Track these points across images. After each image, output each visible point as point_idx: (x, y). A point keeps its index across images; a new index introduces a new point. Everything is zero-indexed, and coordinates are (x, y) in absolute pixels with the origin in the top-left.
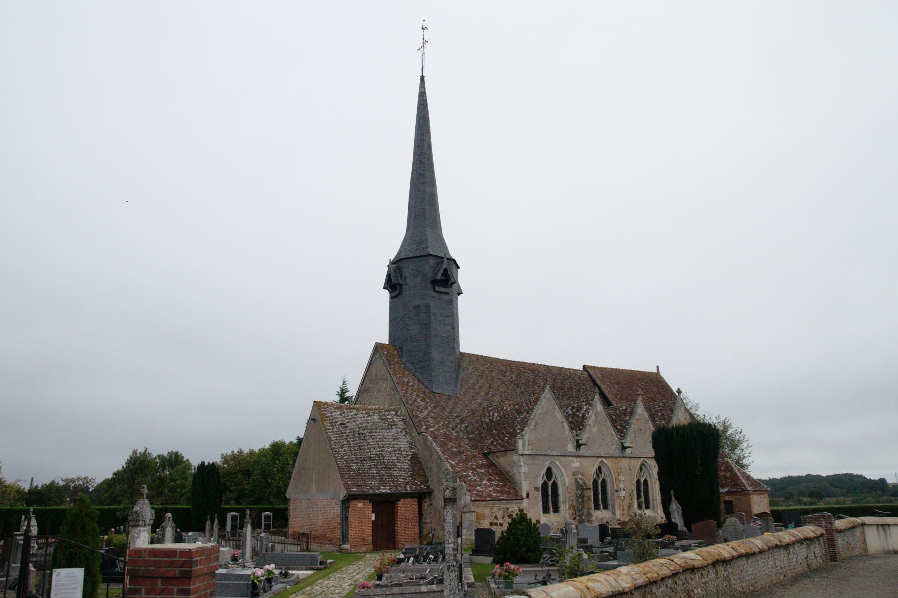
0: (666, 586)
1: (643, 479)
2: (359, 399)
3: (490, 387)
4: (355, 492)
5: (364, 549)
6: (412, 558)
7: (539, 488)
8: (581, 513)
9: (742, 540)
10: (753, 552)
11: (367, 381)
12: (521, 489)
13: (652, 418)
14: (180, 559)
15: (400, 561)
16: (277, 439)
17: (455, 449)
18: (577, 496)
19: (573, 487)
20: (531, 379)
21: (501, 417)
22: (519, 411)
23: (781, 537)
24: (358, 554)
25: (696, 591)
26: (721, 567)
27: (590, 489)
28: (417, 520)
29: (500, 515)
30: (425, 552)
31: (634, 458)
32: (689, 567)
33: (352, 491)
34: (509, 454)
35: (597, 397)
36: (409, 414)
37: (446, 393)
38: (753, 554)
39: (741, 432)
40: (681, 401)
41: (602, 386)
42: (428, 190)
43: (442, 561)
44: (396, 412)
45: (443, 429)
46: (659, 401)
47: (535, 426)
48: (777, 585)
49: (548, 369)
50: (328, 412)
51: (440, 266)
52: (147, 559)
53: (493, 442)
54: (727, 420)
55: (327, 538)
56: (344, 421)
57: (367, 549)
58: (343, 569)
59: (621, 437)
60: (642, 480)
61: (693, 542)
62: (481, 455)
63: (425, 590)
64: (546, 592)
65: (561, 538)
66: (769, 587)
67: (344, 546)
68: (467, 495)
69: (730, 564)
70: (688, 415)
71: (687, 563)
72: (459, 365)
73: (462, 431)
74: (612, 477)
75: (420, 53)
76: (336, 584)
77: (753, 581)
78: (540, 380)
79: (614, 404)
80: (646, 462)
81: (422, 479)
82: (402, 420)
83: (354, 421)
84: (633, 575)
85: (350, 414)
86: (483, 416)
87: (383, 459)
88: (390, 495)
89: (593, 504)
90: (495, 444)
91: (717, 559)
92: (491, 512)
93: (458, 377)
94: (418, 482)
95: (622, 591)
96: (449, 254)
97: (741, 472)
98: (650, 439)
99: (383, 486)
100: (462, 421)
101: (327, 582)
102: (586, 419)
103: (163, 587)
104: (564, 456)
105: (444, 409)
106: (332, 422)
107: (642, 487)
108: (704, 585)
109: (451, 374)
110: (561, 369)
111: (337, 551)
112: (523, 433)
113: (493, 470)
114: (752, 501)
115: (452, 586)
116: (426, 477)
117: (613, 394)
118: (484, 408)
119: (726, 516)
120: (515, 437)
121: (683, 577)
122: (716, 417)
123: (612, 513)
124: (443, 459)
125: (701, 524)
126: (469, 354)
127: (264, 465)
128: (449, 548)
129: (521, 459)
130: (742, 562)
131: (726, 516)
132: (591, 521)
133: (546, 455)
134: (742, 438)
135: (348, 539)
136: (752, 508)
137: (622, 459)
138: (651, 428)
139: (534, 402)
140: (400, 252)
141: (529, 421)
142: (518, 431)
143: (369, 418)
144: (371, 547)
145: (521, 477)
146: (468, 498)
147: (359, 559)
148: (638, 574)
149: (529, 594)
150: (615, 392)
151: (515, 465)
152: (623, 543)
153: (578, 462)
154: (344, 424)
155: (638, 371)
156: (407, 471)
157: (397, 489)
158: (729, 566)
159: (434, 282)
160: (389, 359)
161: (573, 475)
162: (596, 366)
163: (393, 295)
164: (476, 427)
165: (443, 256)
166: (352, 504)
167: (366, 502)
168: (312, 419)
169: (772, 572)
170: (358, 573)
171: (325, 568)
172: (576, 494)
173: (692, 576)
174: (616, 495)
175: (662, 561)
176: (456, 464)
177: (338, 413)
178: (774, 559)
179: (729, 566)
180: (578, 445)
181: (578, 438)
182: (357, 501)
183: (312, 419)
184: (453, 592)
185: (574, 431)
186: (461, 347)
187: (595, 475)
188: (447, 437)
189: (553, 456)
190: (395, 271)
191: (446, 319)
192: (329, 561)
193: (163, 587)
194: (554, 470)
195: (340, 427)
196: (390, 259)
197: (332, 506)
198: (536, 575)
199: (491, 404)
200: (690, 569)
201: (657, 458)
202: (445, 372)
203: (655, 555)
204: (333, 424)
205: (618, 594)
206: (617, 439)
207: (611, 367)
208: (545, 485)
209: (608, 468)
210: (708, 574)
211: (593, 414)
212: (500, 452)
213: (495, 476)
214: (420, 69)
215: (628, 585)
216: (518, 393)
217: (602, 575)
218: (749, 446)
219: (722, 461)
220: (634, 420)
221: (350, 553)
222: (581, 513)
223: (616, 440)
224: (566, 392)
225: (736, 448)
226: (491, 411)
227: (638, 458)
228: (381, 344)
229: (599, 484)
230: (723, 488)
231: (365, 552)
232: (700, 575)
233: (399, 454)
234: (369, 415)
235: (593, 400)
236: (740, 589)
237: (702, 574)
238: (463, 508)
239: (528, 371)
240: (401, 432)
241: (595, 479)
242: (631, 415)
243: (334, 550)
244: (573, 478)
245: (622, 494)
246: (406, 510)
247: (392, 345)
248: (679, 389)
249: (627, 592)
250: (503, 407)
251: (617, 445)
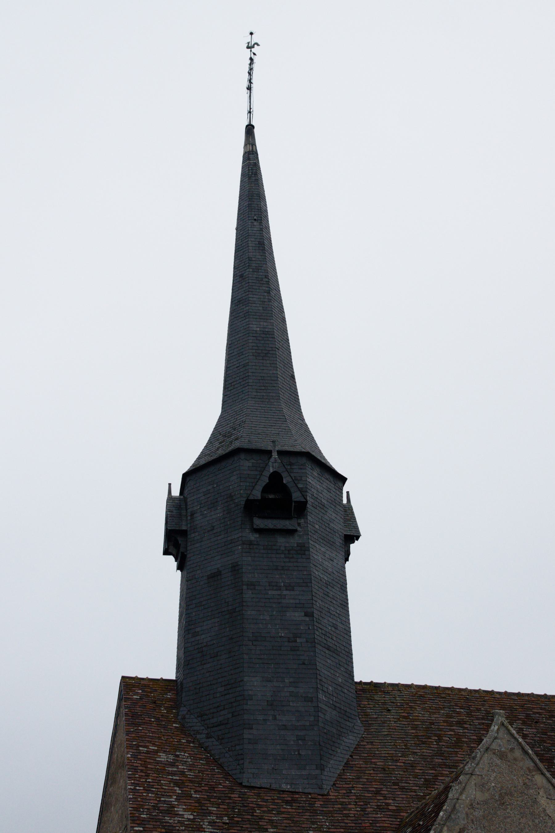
165: (269, 448)
191: (285, 592)
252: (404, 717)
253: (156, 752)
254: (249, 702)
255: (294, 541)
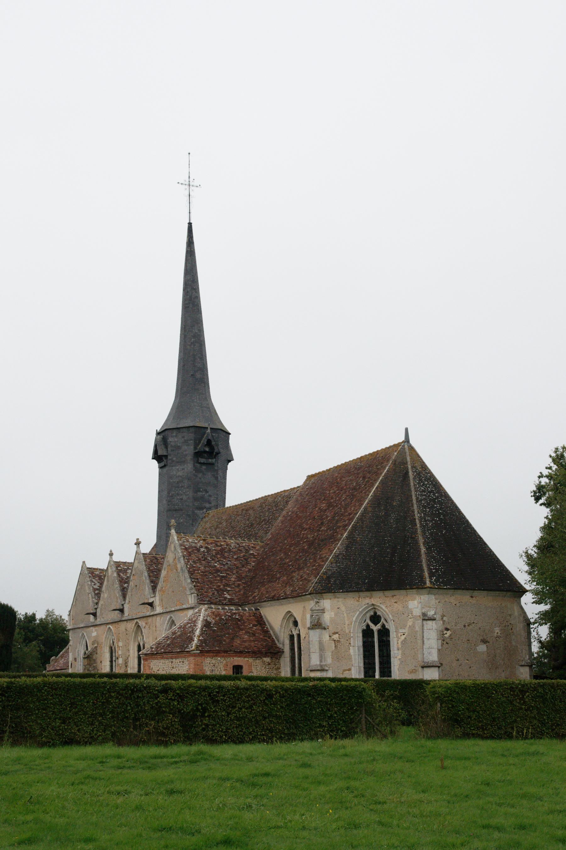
196: (157, 430)
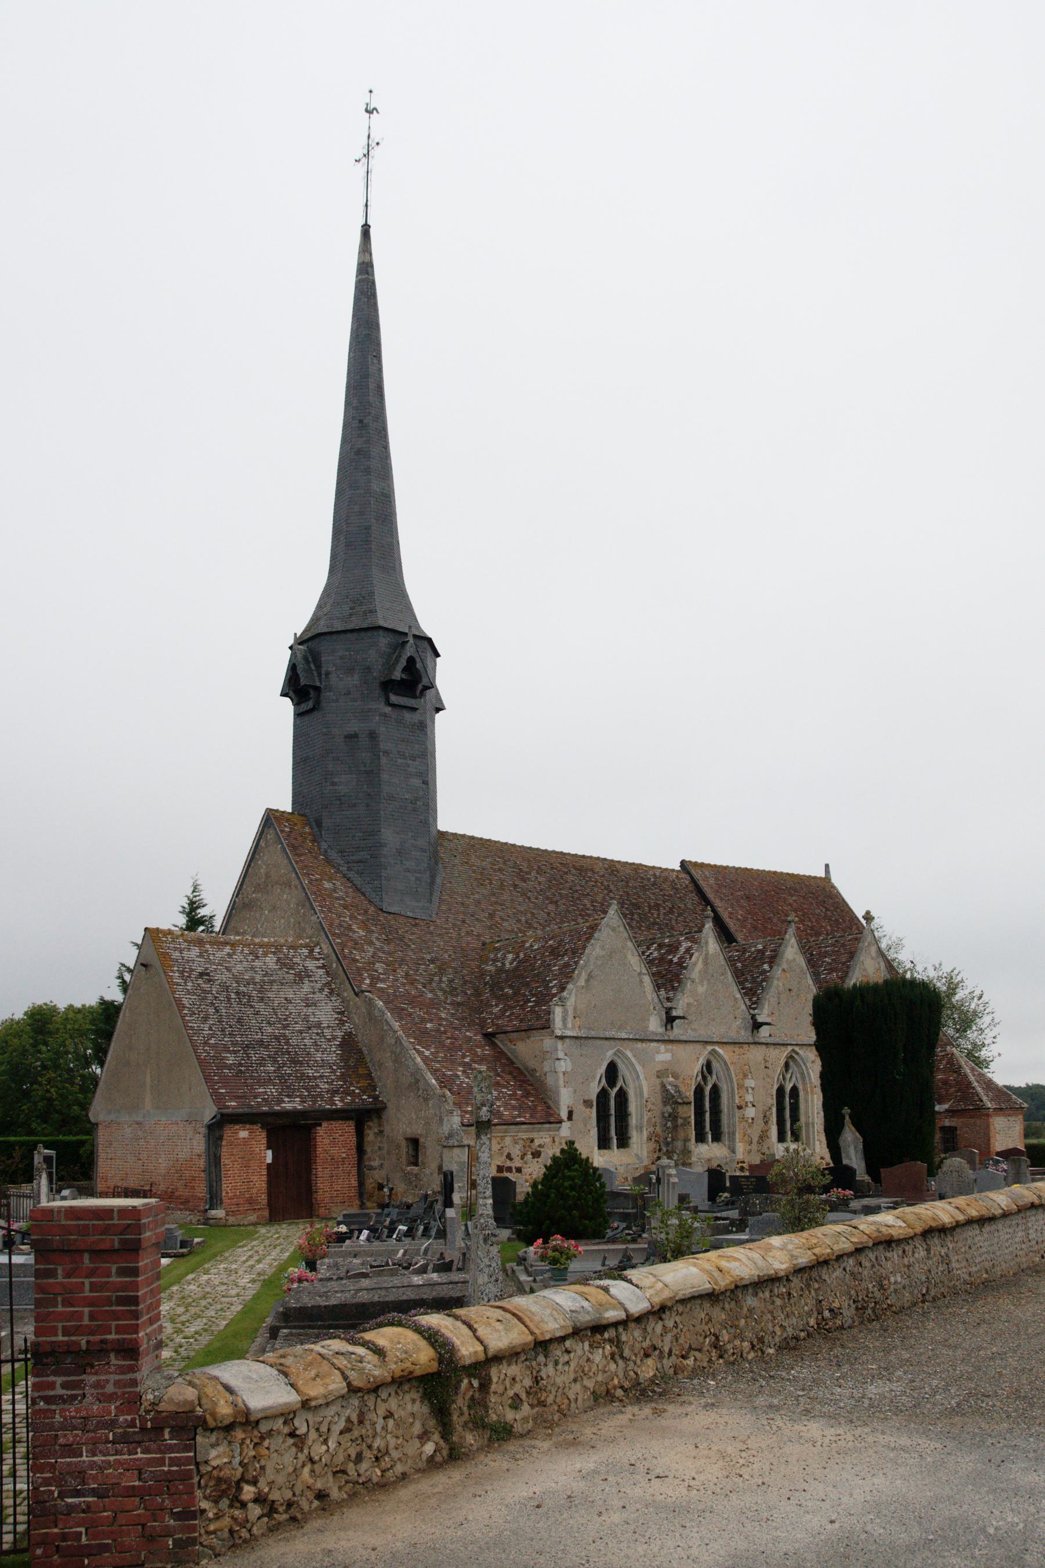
0: (844, 1269)
1: (791, 1085)
2: (232, 924)
3: (496, 903)
4: (234, 1108)
5: (252, 1218)
6: (366, 1233)
7: (592, 1102)
8: (670, 1148)
9: (974, 1196)
10: (991, 1215)
11: (248, 888)
12: (557, 1103)
13: (813, 966)
14: (120, 1222)
15: (341, 1238)
16: (40, 1000)
17: (429, 1025)
18: (664, 1117)
19: (658, 1099)
20: (578, 888)
21: (519, 962)
22: (555, 952)
23: (1040, 1190)
24: (242, 1228)
25: (892, 1279)
26: (936, 1240)
27: (690, 1103)
28: (354, 1160)
29: (516, 1152)
30: (388, 1220)
31: (774, 1044)
32: (883, 1239)
33: (228, 1107)
34: (536, 1036)
35: (709, 926)
36: (336, 954)
37: (409, 914)
38: (992, 1219)
39: (980, 998)
40: (869, 938)
41: (718, 903)
42: (376, 487)
43: (423, 1235)
44: (311, 951)
45: (404, 984)
46: (828, 935)
47: (587, 981)
48: (1029, 1272)
49: (612, 867)
50: (175, 949)
51: (400, 652)
52: (63, 1223)
53: (503, 1011)
54: (956, 972)
55: (179, 1197)
56: (207, 969)
57: (258, 1218)
58: (227, 1254)
59: (753, 1003)
60: (788, 1087)
61: (883, 1201)
62: (479, 1037)
63: (421, 1283)
64: (655, 1276)
65: (646, 1193)
66: (1014, 1274)
67: (213, 1213)
68: (455, 1113)
69: (952, 1236)
70: (882, 964)
71: (880, 1232)
72: (435, 858)
73: (442, 989)
74: (731, 1081)
75: (361, 168)
76: (225, 1281)
77: (988, 1265)
78: (596, 889)
79: (740, 937)
80: (797, 1053)
81: (364, 1083)
82: (323, 967)
83: (227, 968)
84: (791, 1251)
85: (219, 954)
86: (484, 960)
87: (287, 1043)
88: (303, 1114)
89: (694, 1132)
90: (507, 1017)
91: (931, 1226)
92: (499, 1147)
93: (432, 883)
94: (357, 1088)
95: (774, 1276)
96: (418, 627)
97: (976, 1073)
98: (809, 1009)
99: (288, 1096)
100: (442, 970)
101: (206, 1277)
102: (685, 968)
103: (92, 1265)
104: (642, 1040)
105: (406, 944)
106: (183, 971)
107: (787, 1099)
108: (906, 1269)
109: (419, 875)
110: (637, 868)
111: (199, 1222)
112: (565, 994)
113: (503, 1066)
114: (992, 1127)
115: (492, 1269)
116: (372, 1079)
117: (738, 920)
118: (484, 944)
119: (943, 1156)
120: (548, 1002)
121: (872, 1256)
122: (934, 965)
123: (729, 1148)
124: (406, 1044)
125: (898, 1170)
126: (455, 834)
127: (14, 1054)
128: (485, 1205)
129: (560, 1044)
130: (973, 1232)
131: (943, 1156)
132: (690, 1164)
133: (606, 1039)
134: (981, 1008)
135: (221, 1199)
136: (992, 1140)
137: (751, 1046)
138: (810, 990)
139: (585, 933)
140: (315, 620)
141: (576, 972)
142: (554, 991)
143: (257, 963)
144: (266, 1213)
145: (557, 1080)
146: (456, 1120)
147: (250, 1236)
148: (800, 1248)
149: (629, 1277)
150: (741, 915)
151: (548, 1056)
152: (758, 1202)
153: (667, 1051)
154: (208, 974)
155: (788, 874)
156: (335, 1067)
157: (315, 1102)
158: (950, 1238)
159: (388, 686)
160: (294, 842)
161: (658, 1077)
162: (706, 862)
163: (301, 710)
164: (470, 982)
165: (407, 631)
166: (228, 1132)
167: (255, 1127)
168: (143, 965)
169: (1021, 1249)
170: (259, 1261)
171: (190, 1253)
172: (663, 1113)
173: (888, 1255)
174: (737, 1115)
175: (839, 1228)
176: (432, 1053)
177: (195, 951)
178: (1026, 1229)
179: (950, 1238)
180: (670, 1020)
181: (669, 1005)
182: (237, 1127)
183: (143, 965)
184: (494, 1278)
185: (663, 992)
186: (439, 820)
187: (700, 1077)
188: (412, 1001)
189: (622, 1039)
190: (305, 658)
191: (410, 762)
192: (196, 1240)
193: (92, 1265)
194: (621, 1066)
195: (200, 981)
196: (295, 634)
197: (188, 1138)
198: (605, 1258)
199: (499, 936)
200: (886, 1241)
201: (820, 1046)
202: (408, 870)
203: (820, 1220)
204: (186, 974)
205: (767, 1280)
206: (743, 1007)
207: (737, 866)
208: (603, 1095)
209: (726, 1063)
210: (914, 1252)
211: (701, 960)
212: (518, 1031)
213: (509, 1077)
214: (362, 208)
215: (784, 1266)
216: (552, 914)
217: (742, 1250)
218: (993, 1023)
219: (941, 1051)
220: (777, 972)
221: (225, 1226)
222: (670, 1148)
223: (743, 1011)
224: (645, 914)
225: (970, 1027)
226: (498, 949)
227: (783, 1045)
228: (277, 811)
229: (707, 1092)
230: (940, 1103)
231: (255, 1224)
232: (900, 1252)
233: (317, 1034)
234: (257, 957)
235: (700, 931)
236: (967, 1277)
237: (904, 1251)
238: (447, 1138)
239: (573, 871)
240: (321, 990)
241: (699, 1084)
242: (773, 962)
243: (193, 1222)
244: (658, 1081)
245: (750, 1112)
246: (333, 1143)
247: (299, 814)
248: (868, 913)
249: (782, 1277)
250: (524, 942)
251: (743, 1019)
252: (466, 863)
253: (321, 880)
254: (385, 849)
255: (416, 717)
